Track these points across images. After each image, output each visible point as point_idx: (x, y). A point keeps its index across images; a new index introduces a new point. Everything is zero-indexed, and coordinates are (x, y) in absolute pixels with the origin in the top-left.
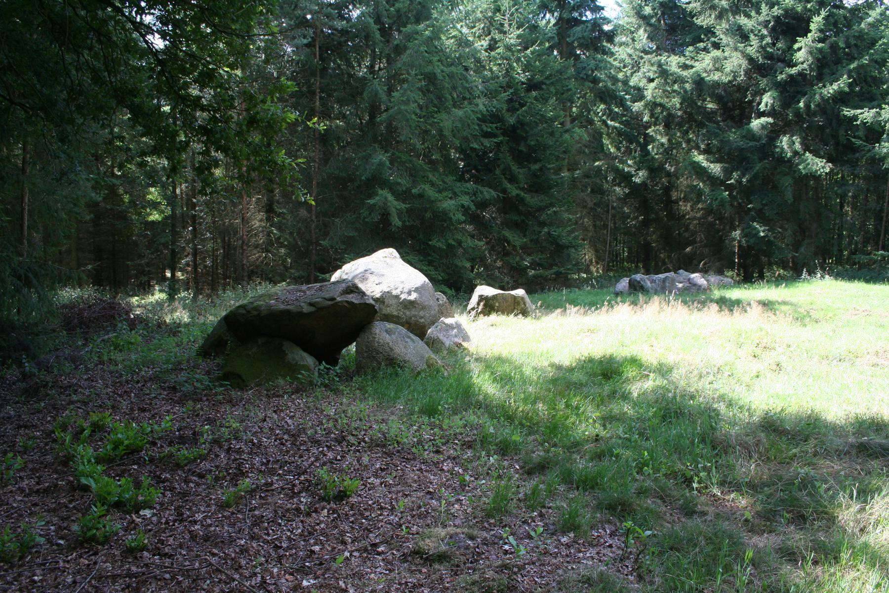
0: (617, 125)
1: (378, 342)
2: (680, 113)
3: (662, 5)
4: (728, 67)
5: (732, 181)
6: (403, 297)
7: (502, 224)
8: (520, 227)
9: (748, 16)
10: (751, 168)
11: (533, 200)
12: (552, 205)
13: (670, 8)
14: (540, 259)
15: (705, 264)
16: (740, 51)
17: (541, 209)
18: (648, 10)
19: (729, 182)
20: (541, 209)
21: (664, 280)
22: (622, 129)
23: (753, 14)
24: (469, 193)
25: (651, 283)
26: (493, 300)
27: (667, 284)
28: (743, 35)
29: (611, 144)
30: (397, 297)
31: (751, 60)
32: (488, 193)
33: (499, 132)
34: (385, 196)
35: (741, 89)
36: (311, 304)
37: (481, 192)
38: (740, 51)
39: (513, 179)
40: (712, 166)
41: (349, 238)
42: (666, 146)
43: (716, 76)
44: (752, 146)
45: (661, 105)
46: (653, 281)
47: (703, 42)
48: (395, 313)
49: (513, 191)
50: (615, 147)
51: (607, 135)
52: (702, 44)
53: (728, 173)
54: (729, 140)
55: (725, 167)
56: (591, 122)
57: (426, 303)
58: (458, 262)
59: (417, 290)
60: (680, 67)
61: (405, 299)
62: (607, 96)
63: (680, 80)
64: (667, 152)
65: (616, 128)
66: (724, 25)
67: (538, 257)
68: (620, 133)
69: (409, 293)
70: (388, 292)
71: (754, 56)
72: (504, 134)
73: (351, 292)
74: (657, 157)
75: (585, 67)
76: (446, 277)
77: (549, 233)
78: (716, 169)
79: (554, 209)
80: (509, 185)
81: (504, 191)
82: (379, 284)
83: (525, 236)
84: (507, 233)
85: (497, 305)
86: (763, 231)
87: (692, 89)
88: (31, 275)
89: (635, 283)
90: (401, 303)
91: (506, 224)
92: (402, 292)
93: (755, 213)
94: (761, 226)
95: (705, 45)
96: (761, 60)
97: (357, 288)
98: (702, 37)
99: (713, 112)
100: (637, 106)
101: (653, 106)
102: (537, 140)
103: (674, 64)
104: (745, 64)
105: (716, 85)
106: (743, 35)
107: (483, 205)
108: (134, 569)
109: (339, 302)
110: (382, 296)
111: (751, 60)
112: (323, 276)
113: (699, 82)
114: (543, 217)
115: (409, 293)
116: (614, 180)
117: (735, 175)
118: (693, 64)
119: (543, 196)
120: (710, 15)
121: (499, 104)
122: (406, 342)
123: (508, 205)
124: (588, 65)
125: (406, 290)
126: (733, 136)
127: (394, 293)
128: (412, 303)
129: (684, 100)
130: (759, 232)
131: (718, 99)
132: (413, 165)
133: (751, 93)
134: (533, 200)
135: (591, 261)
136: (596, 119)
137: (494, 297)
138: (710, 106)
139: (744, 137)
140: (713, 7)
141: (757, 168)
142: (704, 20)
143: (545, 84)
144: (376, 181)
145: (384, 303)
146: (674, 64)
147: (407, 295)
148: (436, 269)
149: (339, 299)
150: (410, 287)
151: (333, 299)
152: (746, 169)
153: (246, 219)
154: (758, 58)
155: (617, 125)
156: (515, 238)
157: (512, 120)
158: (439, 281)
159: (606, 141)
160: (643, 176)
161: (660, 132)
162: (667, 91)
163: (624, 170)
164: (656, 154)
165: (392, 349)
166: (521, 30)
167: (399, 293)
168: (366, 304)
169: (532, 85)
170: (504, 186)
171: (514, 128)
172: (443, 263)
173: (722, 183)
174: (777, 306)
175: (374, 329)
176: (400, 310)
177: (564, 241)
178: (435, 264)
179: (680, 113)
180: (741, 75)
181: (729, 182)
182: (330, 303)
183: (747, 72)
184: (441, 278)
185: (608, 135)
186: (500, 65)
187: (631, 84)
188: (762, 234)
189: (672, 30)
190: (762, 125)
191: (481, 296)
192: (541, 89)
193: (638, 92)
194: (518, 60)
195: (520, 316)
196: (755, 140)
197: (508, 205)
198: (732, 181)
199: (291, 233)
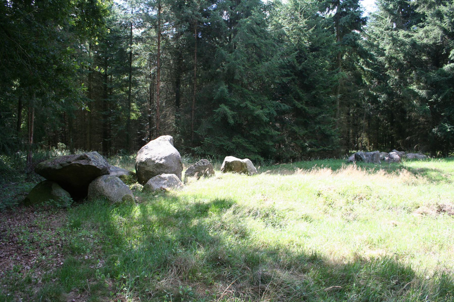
0: (370, 69)
1: (98, 186)
2: (405, 62)
3: (399, 3)
4: (432, 35)
5: (432, 100)
6: (157, 161)
7: (294, 123)
8: (305, 125)
9: (445, 5)
10: (443, 92)
11: (311, 111)
12: (322, 113)
13: (403, 4)
14: (314, 142)
15: (417, 147)
16: (438, 26)
17: (317, 115)
18: (391, 6)
19: (430, 100)
20: (317, 115)
21: (373, 155)
22: (373, 72)
23: (447, 4)
24: (274, 107)
25: (366, 156)
26: (231, 164)
27: (375, 158)
28: (439, 15)
29: (367, 80)
30: (154, 161)
31: (445, 30)
32: (284, 107)
33: (293, 74)
34: (224, 108)
35: (441, 47)
36: (61, 165)
37: (280, 106)
38: (438, 26)
39: (299, 99)
40: (420, 91)
41: (209, 129)
42: (397, 81)
43: (425, 41)
44: (443, 80)
45: (394, 58)
46: (367, 156)
47: (422, 22)
48: (152, 170)
49: (299, 105)
50: (369, 81)
51: (364, 75)
52: (421, 23)
53: (430, 95)
54: (430, 77)
55: (429, 92)
56: (355, 68)
57: (169, 165)
58: (267, 143)
59: (165, 158)
60: (404, 36)
61: (157, 163)
62: (364, 54)
63: (403, 44)
64: (398, 84)
65: (369, 71)
66: (432, 11)
67: (313, 141)
68: (372, 74)
69: (161, 160)
70: (149, 159)
71: (447, 28)
72: (295, 75)
73: (83, 159)
74: (392, 87)
75: (348, 38)
76: (261, 151)
77: (320, 128)
78: (423, 93)
79: (323, 115)
80: (297, 102)
81: (294, 105)
82: (147, 154)
83: (307, 130)
84: (295, 128)
85: (233, 167)
86: (450, 129)
87: (410, 48)
88: (6, 146)
89: (358, 156)
90: (155, 165)
91: (297, 123)
92: (157, 159)
93: (447, 118)
94: (449, 126)
95: (423, 24)
96: (451, 30)
97: (87, 157)
98: (422, 19)
99: (426, 61)
100: (381, 59)
101: (390, 59)
102: (314, 78)
103: (401, 35)
104: (441, 32)
105: (426, 46)
106: (439, 15)
107: (284, 112)
108: (137, 288)
109: (73, 164)
110: (145, 161)
111: (445, 30)
112: (193, 149)
113: (414, 44)
114: (318, 119)
115: (161, 160)
116: (368, 100)
117: (434, 96)
118: (413, 35)
119: (317, 108)
120: (424, 7)
121: (292, 58)
122: (113, 187)
123: (298, 112)
124: (349, 37)
125: (159, 158)
126: (433, 74)
127: (153, 159)
128: (161, 165)
129: (405, 55)
130: (447, 129)
131: (428, 54)
132: (243, 92)
133: (445, 50)
134: (311, 111)
135: (366, 143)
136: (357, 67)
137: (232, 163)
138: (424, 58)
139: (440, 74)
140: (425, 2)
141: (446, 92)
142: (420, 9)
143: (321, 48)
144: (222, 100)
145: (146, 164)
146: (401, 35)
147: (159, 160)
148: (254, 146)
149: (73, 162)
150: (162, 156)
151: (70, 162)
152: (441, 93)
153: (158, 119)
154: (449, 29)
155: (370, 69)
156: (301, 131)
157: (300, 68)
158: (256, 153)
159: (364, 79)
160: (384, 97)
161: (393, 73)
162: (397, 50)
163: (373, 94)
164: (392, 85)
165: (104, 190)
166: (306, 19)
167: (155, 159)
168: (89, 165)
169: (313, 49)
170: (294, 103)
171: (301, 72)
172: (259, 143)
173: (427, 101)
174: (429, 172)
175: (99, 179)
176: (154, 169)
177: (328, 133)
178: (254, 144)
179: (405, 62)
180: (439, 40)
181: (430, 100)
182: (68, 164)
183: (442, 37)
184: (257, 151)
185: (365, 75)
186: (294, 38)
187: (380, 47)
188: (449, 130)
189: (406, 16)
190: (451, 67)
191: (226, 162)
192: (318, 50)
193: (381, 52)
194: (305, 35)
195: (242, 174)
196: (446, 76)
197: (298, 112)
198: (432, 100)
199: (183, 126)
